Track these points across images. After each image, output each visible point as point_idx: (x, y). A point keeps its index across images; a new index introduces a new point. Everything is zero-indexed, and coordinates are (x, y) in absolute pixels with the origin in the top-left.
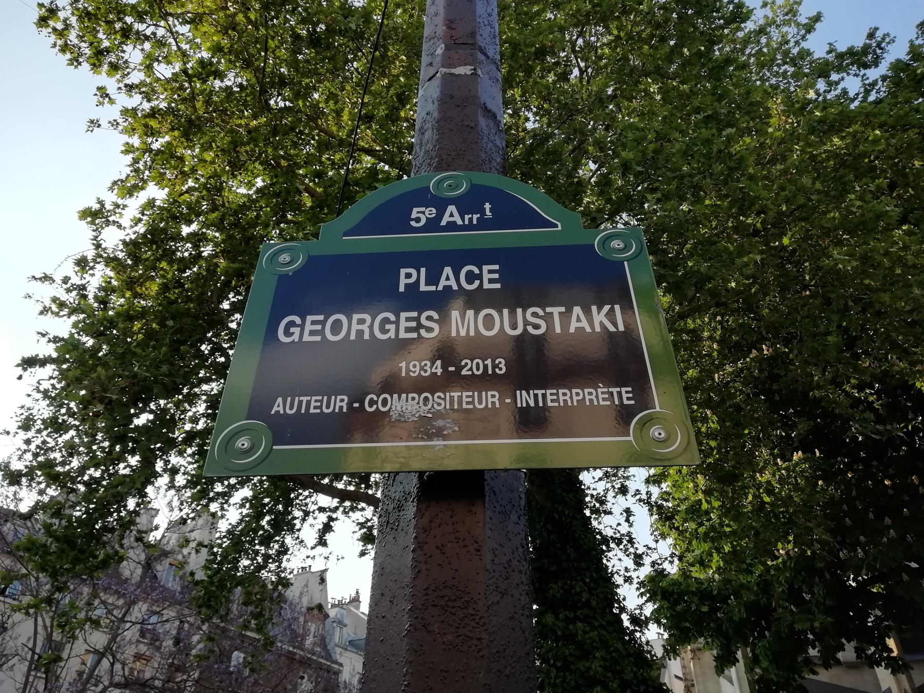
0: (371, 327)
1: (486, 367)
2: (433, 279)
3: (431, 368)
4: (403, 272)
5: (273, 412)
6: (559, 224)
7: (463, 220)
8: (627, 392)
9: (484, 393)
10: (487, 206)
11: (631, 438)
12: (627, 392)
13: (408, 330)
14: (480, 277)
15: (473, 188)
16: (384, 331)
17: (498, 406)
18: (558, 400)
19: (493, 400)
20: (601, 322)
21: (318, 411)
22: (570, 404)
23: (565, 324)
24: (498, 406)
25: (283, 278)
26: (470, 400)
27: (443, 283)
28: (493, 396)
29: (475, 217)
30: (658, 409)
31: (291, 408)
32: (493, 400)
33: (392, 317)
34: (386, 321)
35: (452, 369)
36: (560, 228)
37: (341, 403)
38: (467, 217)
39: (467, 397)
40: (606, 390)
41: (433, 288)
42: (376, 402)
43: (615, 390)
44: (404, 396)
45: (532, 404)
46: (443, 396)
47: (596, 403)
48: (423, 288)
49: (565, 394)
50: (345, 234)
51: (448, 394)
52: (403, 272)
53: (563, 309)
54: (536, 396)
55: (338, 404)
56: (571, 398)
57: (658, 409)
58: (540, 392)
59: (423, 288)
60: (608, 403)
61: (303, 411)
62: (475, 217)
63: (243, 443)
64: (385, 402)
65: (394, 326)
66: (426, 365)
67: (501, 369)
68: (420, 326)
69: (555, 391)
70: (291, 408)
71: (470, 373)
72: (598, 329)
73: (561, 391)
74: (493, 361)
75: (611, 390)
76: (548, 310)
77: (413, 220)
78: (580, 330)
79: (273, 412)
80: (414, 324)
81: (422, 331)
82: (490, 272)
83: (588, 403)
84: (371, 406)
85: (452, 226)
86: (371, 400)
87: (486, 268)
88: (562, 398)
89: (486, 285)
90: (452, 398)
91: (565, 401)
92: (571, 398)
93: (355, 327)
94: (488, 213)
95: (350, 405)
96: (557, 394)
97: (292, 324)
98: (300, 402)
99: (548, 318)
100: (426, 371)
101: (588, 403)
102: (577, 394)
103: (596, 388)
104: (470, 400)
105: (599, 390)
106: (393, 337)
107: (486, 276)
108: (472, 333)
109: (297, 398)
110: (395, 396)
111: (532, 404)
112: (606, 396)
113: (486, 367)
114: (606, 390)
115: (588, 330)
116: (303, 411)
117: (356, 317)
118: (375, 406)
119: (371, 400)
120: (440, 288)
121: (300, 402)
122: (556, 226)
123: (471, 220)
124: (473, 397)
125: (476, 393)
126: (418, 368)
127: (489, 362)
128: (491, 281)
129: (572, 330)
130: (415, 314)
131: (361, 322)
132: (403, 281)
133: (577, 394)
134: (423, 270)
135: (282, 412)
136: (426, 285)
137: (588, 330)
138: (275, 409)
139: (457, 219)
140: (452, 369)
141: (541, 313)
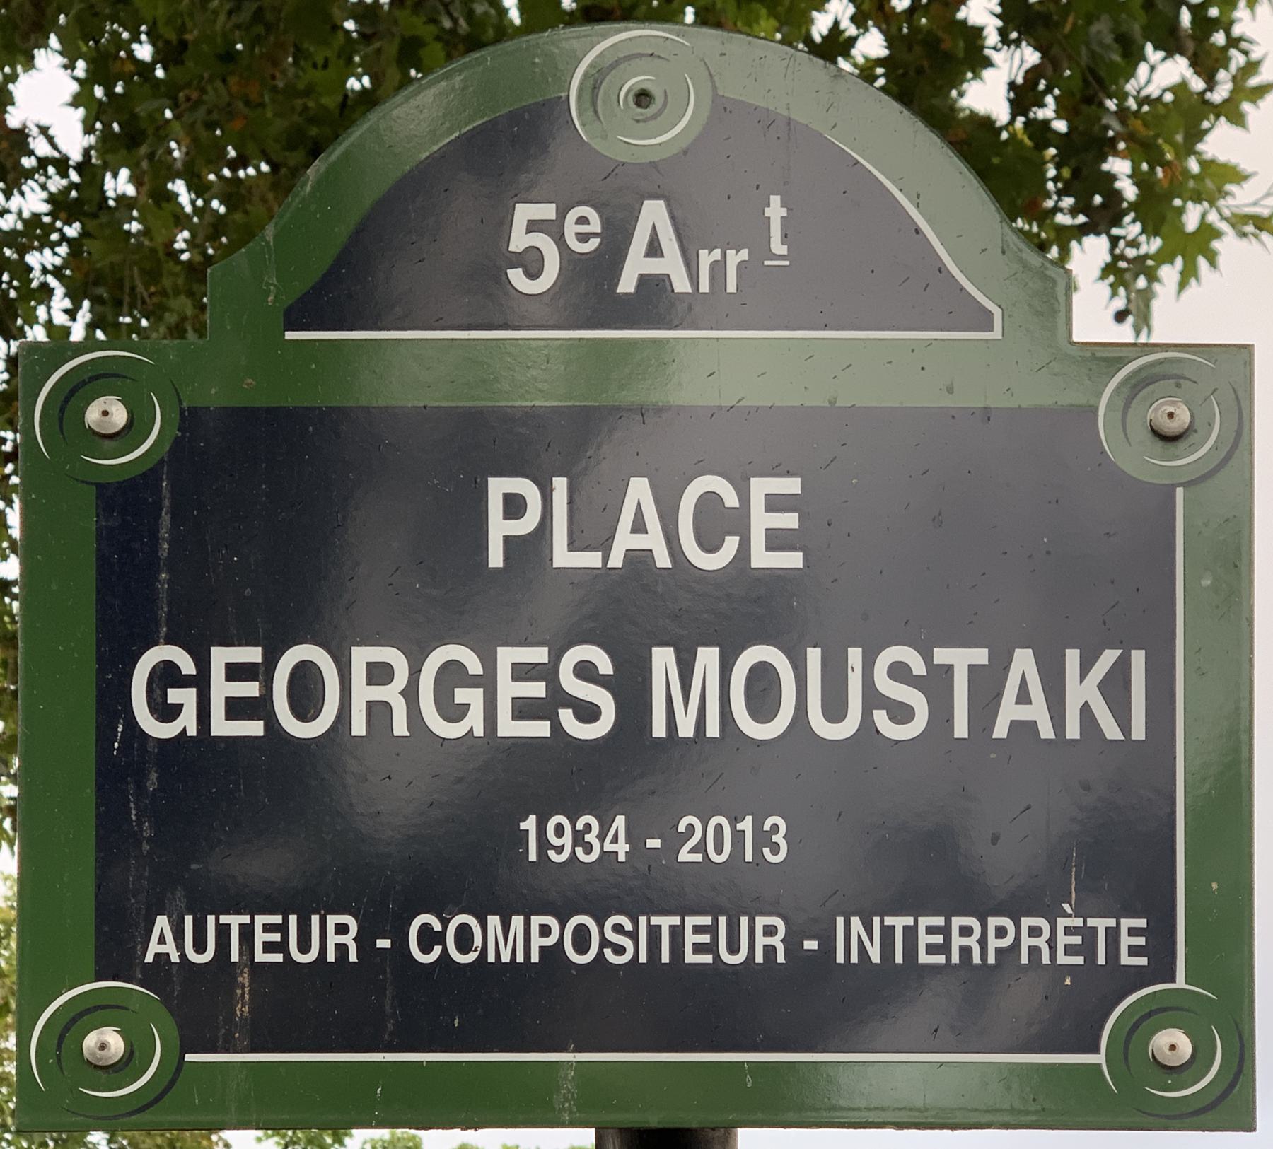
0: (410, 693)
1: (738, 837)
3: (602, 837)
4: (498, 487)
8: (1132, 932)
11: (1099, 1059)
12: (1132, 932)
13: (523, 709)
14: (739, 522)
17: (353, 957)
18: (945, 949)
19: (341, 939)
20: (1086, 710)
21: (708, 959)
22: (977, 959)
23: (985, 704)
24: (353, 957)
26: (706, 938)
27: (624, 541)
28: (342, 929)
29: (735, 258)
30: (1180, 982)
32: (341, 939)
34: (452, 674)
39: (268, 928)
40: (1078, 922)
41: (591, 559)
42: (440, 938)
43: (1101, 924)
44: (517, 921)
45: (875, 955)
46: (628, 926)
47: (1046, 960)
48: (563, 557)
49: (966, 931)
51: (643, 920)
52: (498, 487)
53: (980, 656)
54: (888, 932)
56: (983, 942)
57: (1180, 982)
58: (899, 923)
59: (563, 557)
60: (1079, 960)
61: (665, 958)
62: (735, 258)
65: (192, 692)
66: (588, 827)
68: (559, 698)
69: (939, 921)
71: (698, 857)
72: (1073, 730)
73: (957, 922)
74: (758, 827)
76: (942, 656)
80: (537, 690)
83: (1024, 959)
84: (426, 949)
86: (425, 928)
88: (957, 941)
89: (762, 559)
90: (654, 932)
92: (983, 942)
95: (792, 943)
96: (946, 931)
98: (223, 931)
100: (588, 849)
101: (1024, 959)
102: (545, 931)
103: (1052, 915)
105: (1062, 923)
106: (192, 731)
107: (762, 521)
109: (211, 919)
110: (494, 921)
111: (875, 955)
112: (1077, 940)
113: (738, 837)
114: (1078, 922)
115: (1046, 731)
116: (665, 958)
118: (437, 950)
119: (425, 928)
124: (283, 929)
125: (293, 919)
126: (567, 839)
127: (746, 825)
128: (776, 541)
129: (1001, 730)
132: (499, 528)
133: (1001, 932)
134: (560, 485)
135: (175, 958)
138: (154, 948)
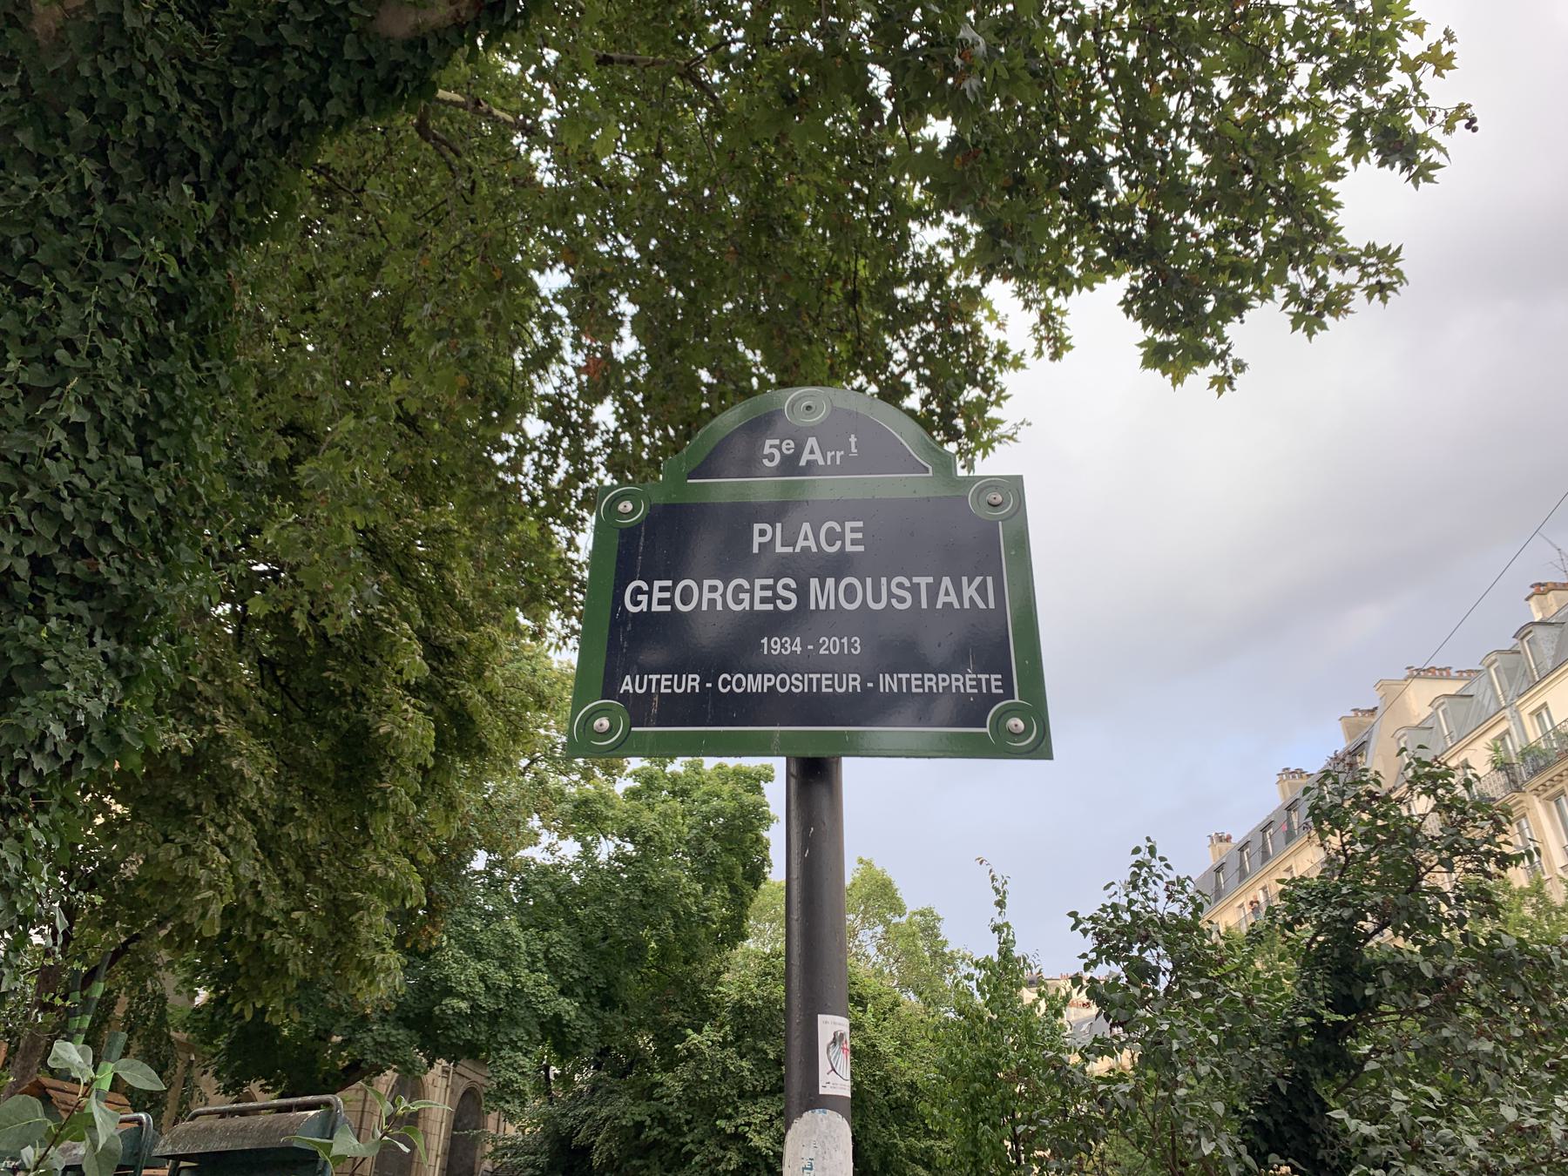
0: (724, 595)
1: (842, 645)
4: (757, 527)
7: (825, 460)
10: (853, 439)
11: (987, 730)
13: (764, 600)
14: (842, 536)
16: (739, 602)
18: (922, 686)
20: (971, 598)
27: (801, 543)
29: (839, 454)
30: (1017, 700)
31: (641, 687)
33: (645, 587)
34: (739, 588)
37: (692, 682)
41: (790, 550)
43: (984, 677)
44: (759, 676)
48: (779, 549)
52: (757, 527)
53: (930, 580)
54: (900, 680)
55: (690, 683)
57: (1017, 700)
58: (904, 676)
59: (779, 549)
62: (839, 454)
63: (603, 723)
68: (776, 596)
70: (641, 687)
72: (967, 605)
76: (915, 580)
77: (766, 457)
78: (948, 605)
80: (769, 593)
81: (779, 602)
82: (853, 530)
87: (848, 525)
88: (927, 683)
90: (810, 680)
93: (707, 595)
96: (922, 679)
98: (650, 681)
99: (914, 590)
107: (849, 536)
110: (750, 676)
113: (842, 645)
115: (957, 606)
117: (707, 583)
120: (798, 550)
121: (650, 681)
122: (927, 470)
127: (845, 640)
128: (854, 542)
129: (939, 606)
130: (770, 582)
131: (713, 589)
132: (757, 540)
134: (779, 526)
137: (957, 606)
138: (624, 687)
141: (907, 584)
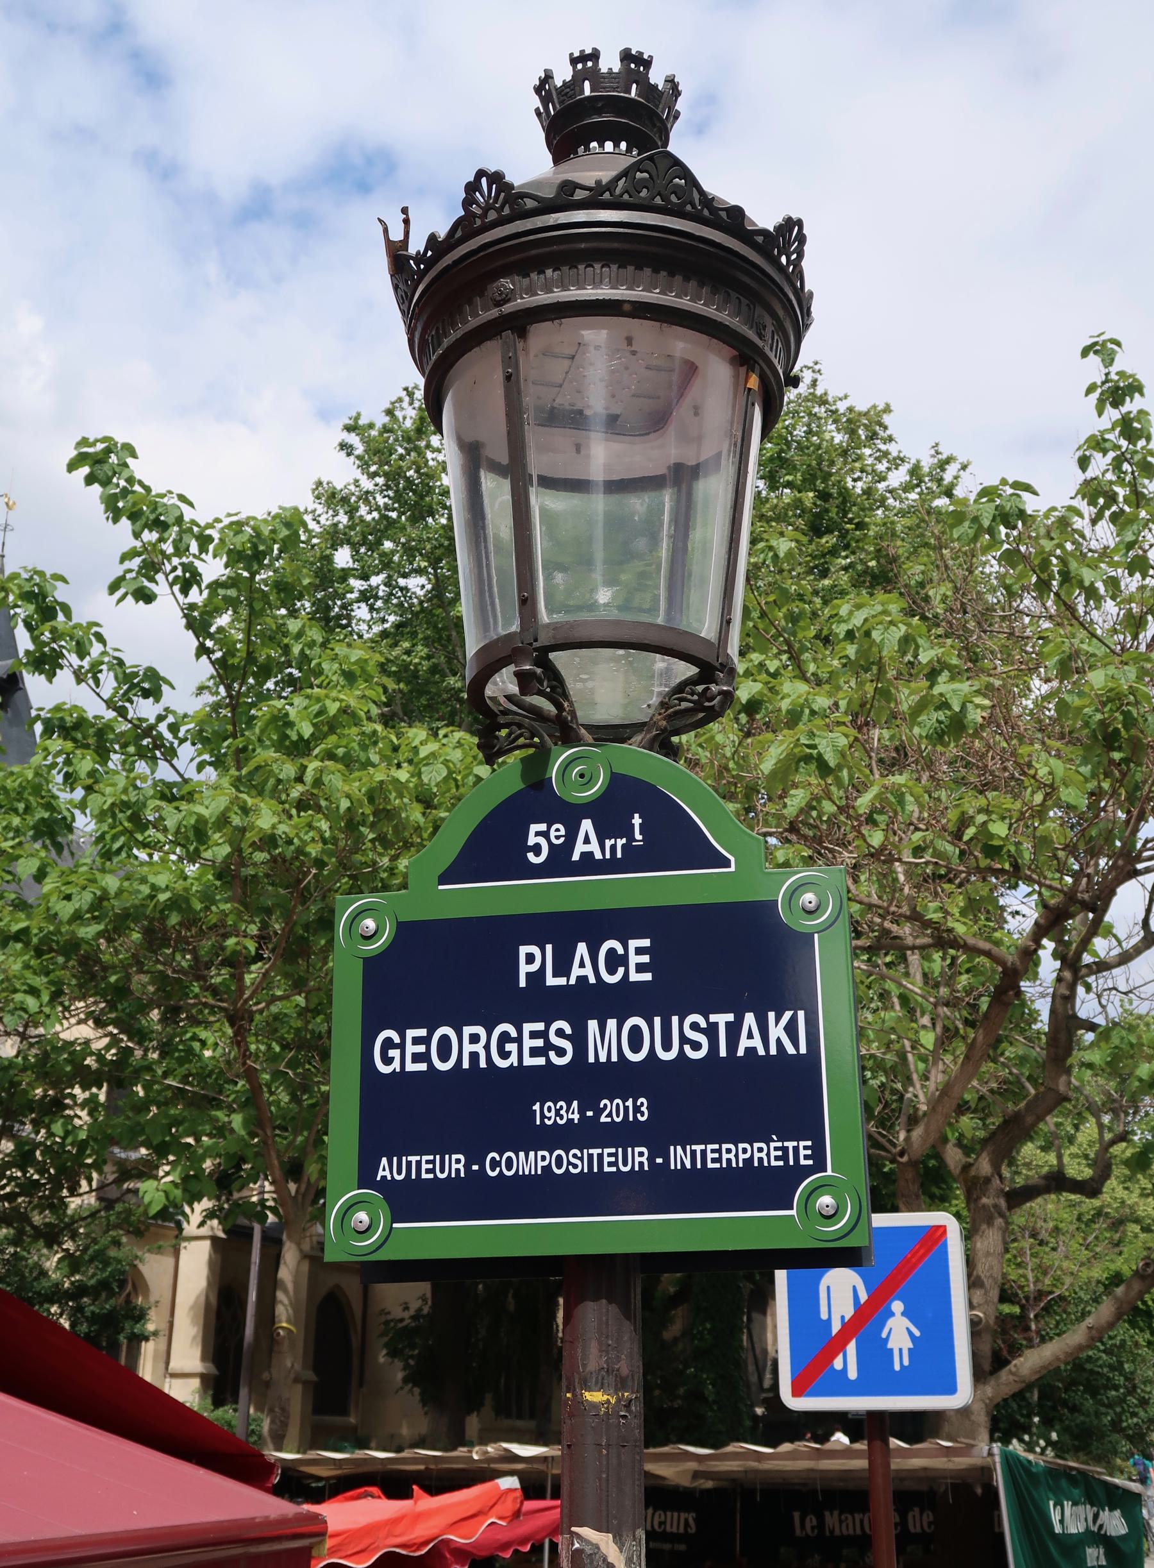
0: (487, 1047)
1: (626, 1109)
2: (562, 967)
3: (567, 1112)
4: (524, 950)
5: (378, 1178)
6: (732, 859)
8: (805, 1148)
9: (447, 1157)
10: (637, 820)
12: (805, 1148)
13: (534, 1052)
14: (623, 960)
15: (617, 781)
22: (734, 1165)
25: (370, 963)
27: (576, 972)
29: (621, 842)
35: (590, 1114)
36: (733, 869)
38: (608, 843)
40: (779, 1144)
41: (562, 981)
42: (499, 1164)
47: (766, 1164)
48: (551, 981)
49: (729, 1151)
50: (443, 880)
51: (585, 1151)
52: (524, 950)
53: (730, 1017)
54: (693, 1153)
56: (737, 1156)
57: (829, 1172)
58: (698, 1148)
59: (551, 981)
62: (621, 842)
64: (509, 1162)
66: (561, 1107)
67: (642, 1115)
68: (549, 1046)
69: (716, 1146)
71: (609, 1120)
73: (725, 1146)
74: (634, 1103)
75: (786, 1144)
79: (378, 1178)
83: (756, 1164)
84: (493, 1170)
85: (588, 864)
87: (633, 944)
88: (725, 1156)
89: (634, 977)
90: (590, 1156)
91: (728, 1161)
92: (737, 1156)
94: (638, 836)
96: (719, 1151)
97: (388, 1044)
98: (409, 1163)
101: (756, 1164)
102: (745, 1151)
104: (430, 1166)
105: (772, 1145)
107: (634, 959)
108: (614, 1058)
112: (780, 1153)
113: (626, 1109)
114: (779, 1144)
118: (498, 1169)
121: (409, 1163)
122: (727, 864)
123: (613, 848)
125: (620, 1150)
126: (553, 1114)
127: (630, 1103)
128: (640, 968)
132: (524, 969)
133: (745, 1151)
134: (549, 948)
136: (554, 976)
138: (381, 1173)
139: (594, 847)
140: (590, 1114)
